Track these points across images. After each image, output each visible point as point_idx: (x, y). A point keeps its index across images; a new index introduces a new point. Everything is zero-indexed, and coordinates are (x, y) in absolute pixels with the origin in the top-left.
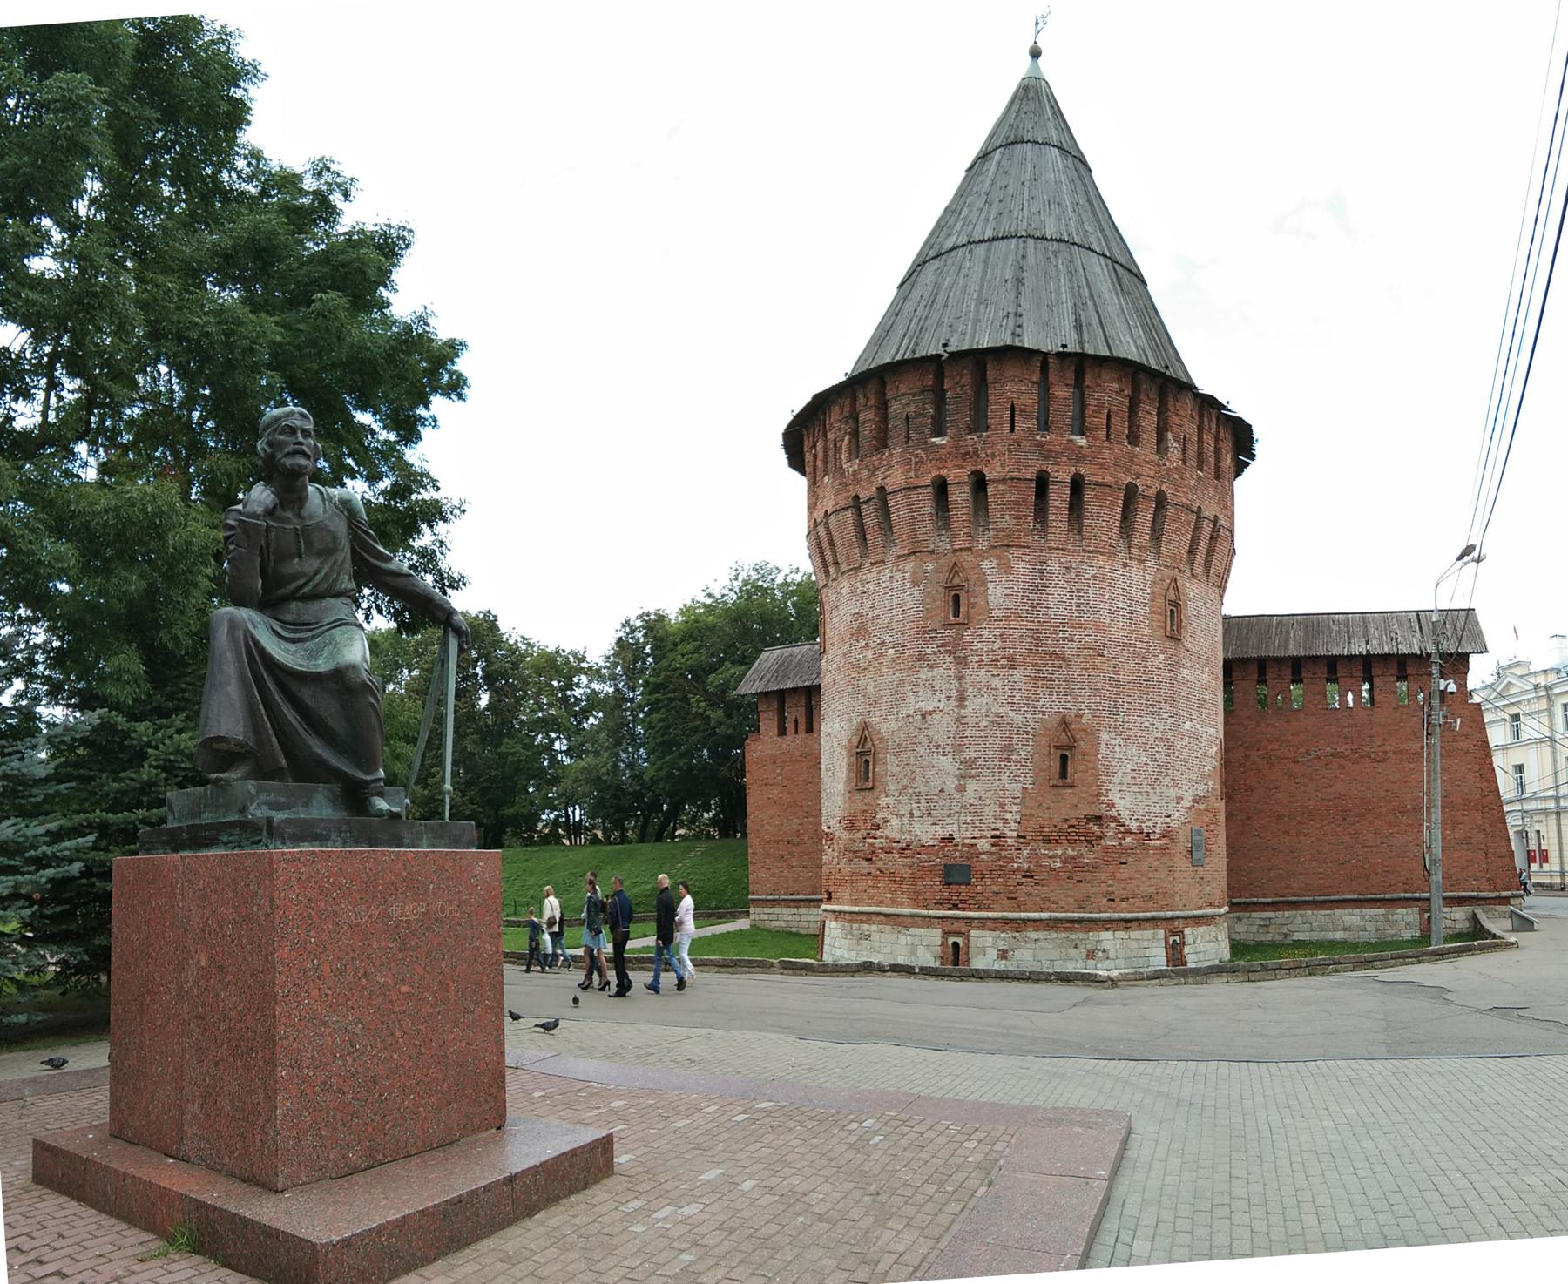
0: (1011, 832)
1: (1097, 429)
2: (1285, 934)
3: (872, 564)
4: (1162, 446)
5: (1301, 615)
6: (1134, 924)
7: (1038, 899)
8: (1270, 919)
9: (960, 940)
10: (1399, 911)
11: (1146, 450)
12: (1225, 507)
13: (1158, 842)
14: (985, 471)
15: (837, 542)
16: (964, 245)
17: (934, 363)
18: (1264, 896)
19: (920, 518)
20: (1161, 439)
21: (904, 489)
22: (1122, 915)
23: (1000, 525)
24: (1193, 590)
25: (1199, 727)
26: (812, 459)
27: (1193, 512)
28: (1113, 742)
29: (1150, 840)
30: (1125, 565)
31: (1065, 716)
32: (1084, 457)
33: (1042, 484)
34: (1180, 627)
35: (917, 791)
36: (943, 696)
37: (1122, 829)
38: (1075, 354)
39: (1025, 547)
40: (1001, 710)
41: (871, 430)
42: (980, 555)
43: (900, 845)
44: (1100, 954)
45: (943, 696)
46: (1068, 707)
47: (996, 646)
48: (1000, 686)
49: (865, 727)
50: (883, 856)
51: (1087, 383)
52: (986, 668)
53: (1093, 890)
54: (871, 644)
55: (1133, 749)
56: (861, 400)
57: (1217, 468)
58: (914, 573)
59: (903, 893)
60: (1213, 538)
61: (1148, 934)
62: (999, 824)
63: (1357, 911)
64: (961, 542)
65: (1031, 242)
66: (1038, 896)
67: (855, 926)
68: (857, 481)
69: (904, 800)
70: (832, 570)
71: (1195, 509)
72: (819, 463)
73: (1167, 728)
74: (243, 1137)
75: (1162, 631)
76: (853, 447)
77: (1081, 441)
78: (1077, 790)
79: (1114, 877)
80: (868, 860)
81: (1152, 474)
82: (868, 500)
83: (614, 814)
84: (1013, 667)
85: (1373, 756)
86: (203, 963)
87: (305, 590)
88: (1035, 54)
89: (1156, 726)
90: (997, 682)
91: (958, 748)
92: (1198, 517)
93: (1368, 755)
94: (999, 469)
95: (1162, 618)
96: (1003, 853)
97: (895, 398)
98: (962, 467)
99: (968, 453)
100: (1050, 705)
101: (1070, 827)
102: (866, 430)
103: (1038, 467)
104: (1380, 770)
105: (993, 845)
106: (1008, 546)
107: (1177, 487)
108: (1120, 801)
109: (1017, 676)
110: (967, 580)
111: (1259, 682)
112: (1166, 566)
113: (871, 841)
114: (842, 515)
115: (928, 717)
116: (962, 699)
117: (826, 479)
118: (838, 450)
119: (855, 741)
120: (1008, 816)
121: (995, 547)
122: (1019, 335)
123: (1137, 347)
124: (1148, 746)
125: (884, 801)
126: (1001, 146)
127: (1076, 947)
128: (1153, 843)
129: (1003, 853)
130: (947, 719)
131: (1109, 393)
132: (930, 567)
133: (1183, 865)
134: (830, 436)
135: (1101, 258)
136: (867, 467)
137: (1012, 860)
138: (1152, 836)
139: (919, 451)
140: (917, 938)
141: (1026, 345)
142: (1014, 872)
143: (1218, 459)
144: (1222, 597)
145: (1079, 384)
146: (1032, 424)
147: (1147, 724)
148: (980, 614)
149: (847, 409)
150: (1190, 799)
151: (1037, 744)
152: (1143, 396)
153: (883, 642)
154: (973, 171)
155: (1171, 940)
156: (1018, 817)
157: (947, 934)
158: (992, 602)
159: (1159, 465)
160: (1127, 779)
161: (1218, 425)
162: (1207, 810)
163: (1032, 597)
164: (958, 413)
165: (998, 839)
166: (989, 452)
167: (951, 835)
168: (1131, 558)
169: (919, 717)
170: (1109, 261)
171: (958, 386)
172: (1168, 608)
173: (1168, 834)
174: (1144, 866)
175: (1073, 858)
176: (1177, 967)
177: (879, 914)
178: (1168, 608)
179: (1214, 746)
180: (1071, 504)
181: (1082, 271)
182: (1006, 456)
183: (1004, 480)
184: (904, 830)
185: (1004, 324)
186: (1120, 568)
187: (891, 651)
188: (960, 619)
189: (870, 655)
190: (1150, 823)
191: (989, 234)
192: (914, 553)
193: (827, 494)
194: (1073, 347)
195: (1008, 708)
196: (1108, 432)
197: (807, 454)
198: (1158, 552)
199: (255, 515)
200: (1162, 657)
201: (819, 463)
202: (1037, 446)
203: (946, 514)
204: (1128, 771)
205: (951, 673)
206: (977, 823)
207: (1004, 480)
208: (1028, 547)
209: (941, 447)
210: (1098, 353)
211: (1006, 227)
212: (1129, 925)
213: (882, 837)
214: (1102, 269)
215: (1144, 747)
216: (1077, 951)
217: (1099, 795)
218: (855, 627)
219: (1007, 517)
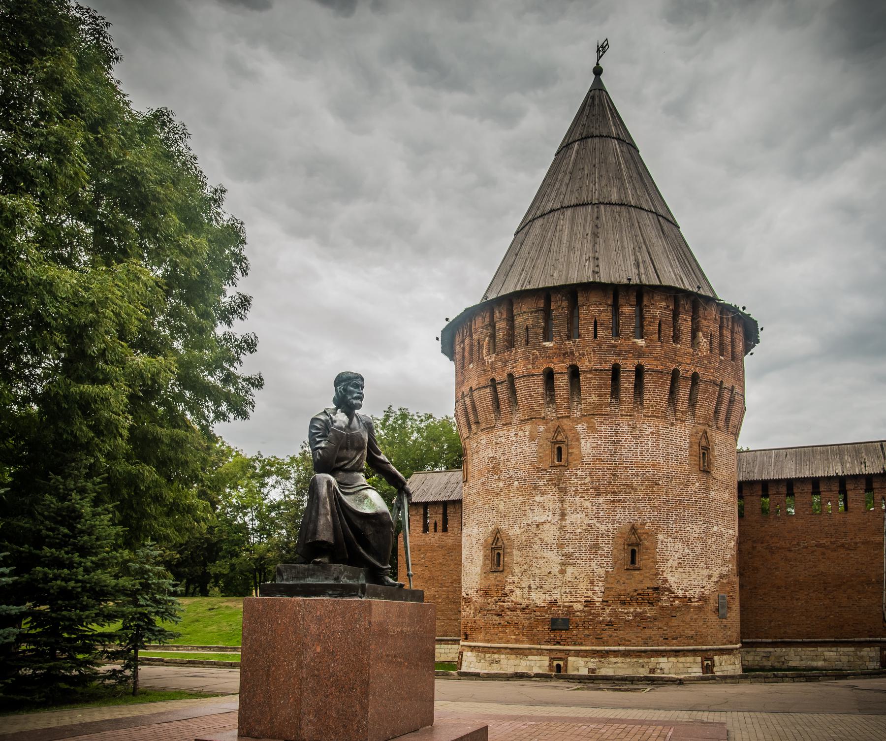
0: (598, 598)
1: (652, 334)
3: (504, 425)
4: (695, 342)
5: (792, 448)
6: (681, 653)
7: (616, 639)
9: (561, 663)
10: (865, 649)
11: (684, 347)
12: (739, 380)
13: (697, 604)
14: (579, 364)
16: (558, 209)
17: (546, 294)
18: (767, 638)
20: (694, 336)
21: (525, 376)
22: (673, 648)
23: (588, 401)
24: (718, 438)
25: (722, 529)
26: (461, 351)
27: (717, 385)
30: (672, 424)
31: (633, 525)
32: (644, 353)
33: (616, 371)
34: (710, 463)
37: (673, 595)
38: (637, 285)
39: (605, 415)
40: (591, 522)
41: (504, 335)
42: (575, 421)
43: (522, 606)
44: (659, 671)
46: (636, 518)
47: (587, 481)
48: (590, 507)
49: (497, 532)
50: (509, 613)
51: (644, 303)
53: (654, 633)
54: (502, 478)
55: (679, 545)
57: (733, 352)
58: (531, 432)
60: (731, 402)
61: (690, 659)
62: (590, 594)
63: (834, 649)
64: (562, 412)
65: (602, 207)
66: (616, 636)
67: (487, 655)
68: (493, 369)
69: (525, 578)
70: (473, 427)
71: (718, 383)
72: (466, 354)
75: (697, 467)
76: (491, 346)
77: (641, 342)
78: (642, 572)
79: (667, 625)
80: (499, 615)
81: (689, 362)
82: (502, 382)
84: (599, 494)
85: (847, 546)
86: (318, 650)
89: (695, 530)
90: (587, 504)
91: (560, 546)
92: (721, 388)
93: (843, 546)
94: (587, 364)
95: (697, 459)
96: (593, 611)
97: (519, 314)
98: (563, 362)
99: (567, 353)
100: (624, 518)
101: (638, 594)
102: (500, 335)
103: (613, 362)
104: (852, 555)
105: (585, 606)
106: (593, 415)
107: (706, 369)
109: (601, 500)
110: (566, 437)
111: (762, 496)
112: (699, 424)
113: (501, 604)
114: (482, 392)
115: (541, 527)
116: (563, 515)
117: (471, 366)
118: (480, 347)
119: (490, 540)
120: (596, 588)
121: (585, 415)
122: (597, 273)
123: (675, 275)
125: (510, 579)
126: (578, 140)
127: (643, 667)
128: (693, 604)
129: (593, 611)
130: (554, 527)
131: (658, 309)
132: (542, 428)
133: (713, 618)
134: (475, 337)
135: (650, 214)
136: (501, 360)
137: (599, 615)
139: (535, 351)
141: (603, 281)
142: (600, 622)
143: (733, 347)
144: (736, 440)
147: (688, 529)
149: (487, 320)
150: (717, 576)
151: (615, 543)
152: (681, 309)
153: (511, 477)
154: (560, 156)
155: (706, 663)
156: (603, 589)
157: (552, 660)
158: (584, 452)
159: (693, 355)
160: (675, 564)
162: (728, 583)
163: (611, 448)
164: (559, 325)
165: (589, 603)
168: (676, 420)
169: (535, 526)
170: (655, 216)
171: (559, 307)
172: (702, 451)
173: (703, 599)
174: (688, 619)
175: (640, 613)
176: (709, 675)
177: (506, 648)
178: (702, 451)
180: (635, 385)
181: (637, 224)
183: (590, 371)
185: (587, 264)
187: (516, 483)
188: (562, 463)
189: (501, 484)
190: (691, 592)
191: (573, 202)
192: (531, 419)
194: (635, 281)
195: (595, 521)
196: (659, 335)
197: (458, 347)
198: (694, 415)
199: (341, 428)
200: (697, 484)
201: (466, 354)
203: (552, 393)
204: (676, 558)
205: (556, 498)
206: (573, 593)
207: (590, 371)
208: (607, 415)
209: (550, 348)
210: (651, 283)
211: (584, 197)
212: (678, 654)
213: (509, 602)
214: (650, 221)
215: (687, 543)
216: (644, 669)
217: (657, 574)
218: (491, 466)
219: (593, 396)
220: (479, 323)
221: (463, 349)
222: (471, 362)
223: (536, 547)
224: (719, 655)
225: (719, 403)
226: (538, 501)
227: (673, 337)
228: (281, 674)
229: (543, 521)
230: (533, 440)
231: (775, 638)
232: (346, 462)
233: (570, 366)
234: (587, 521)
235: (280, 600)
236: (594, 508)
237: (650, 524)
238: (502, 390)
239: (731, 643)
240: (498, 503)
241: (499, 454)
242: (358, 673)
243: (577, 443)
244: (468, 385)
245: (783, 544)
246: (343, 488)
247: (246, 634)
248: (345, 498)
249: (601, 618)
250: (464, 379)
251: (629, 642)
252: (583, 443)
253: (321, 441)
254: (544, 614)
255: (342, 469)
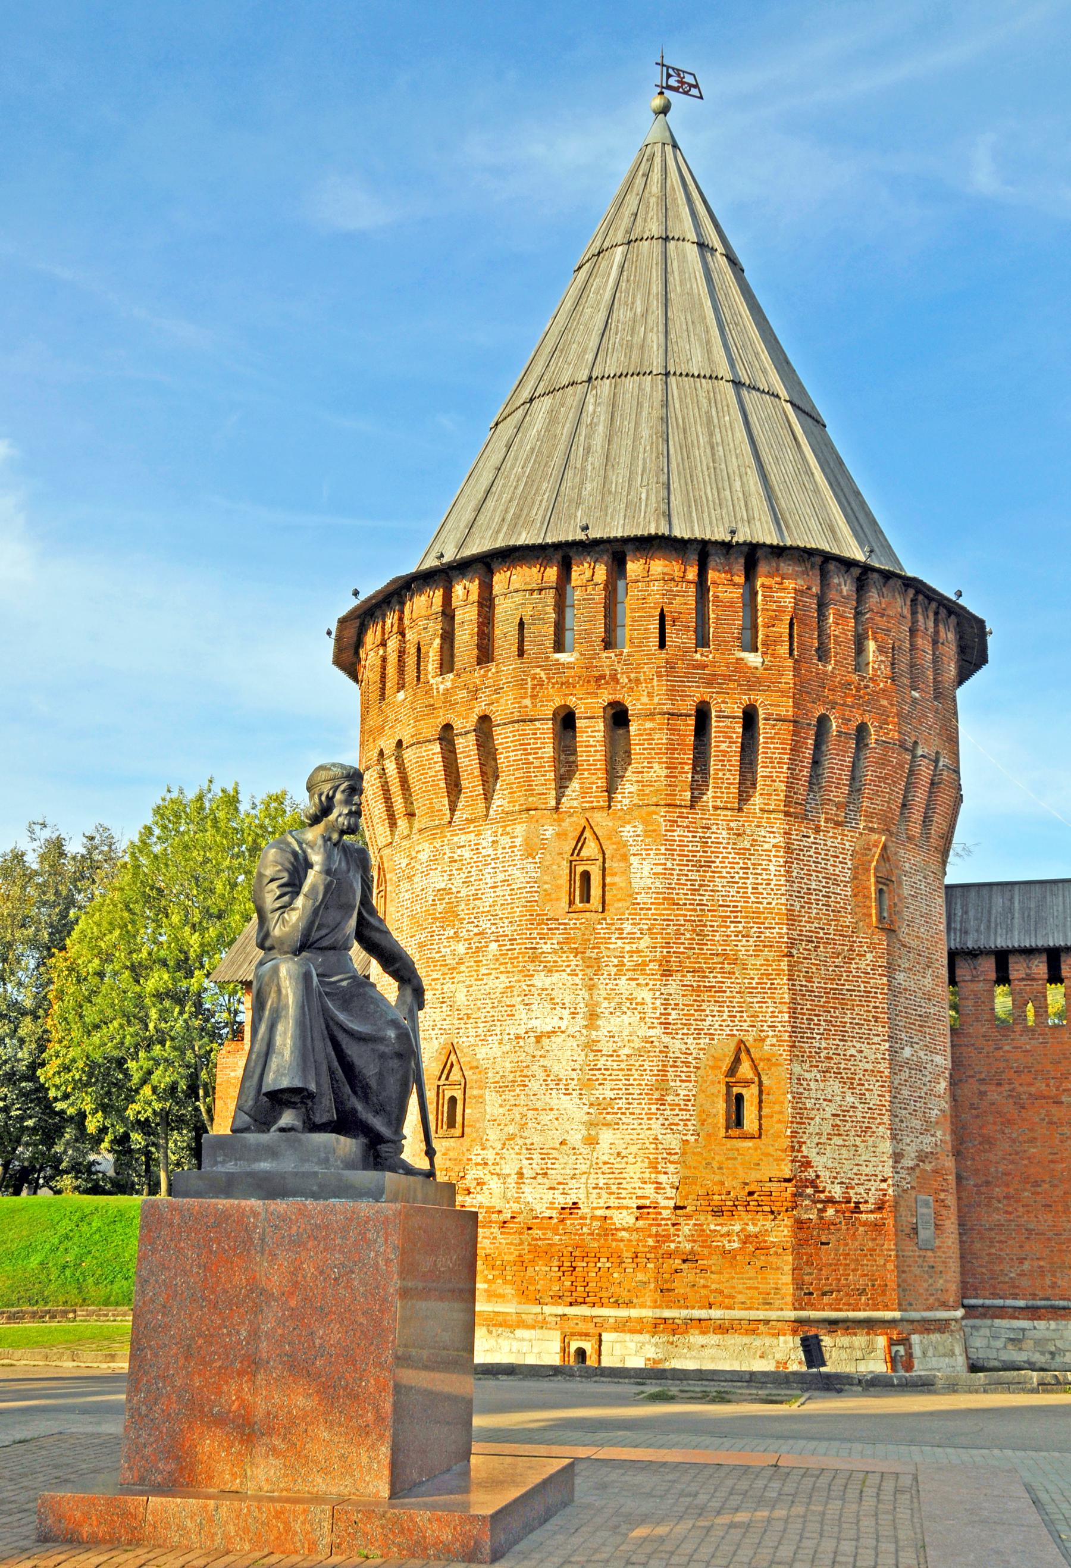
2: (1052, 1354)
8: (1023, 1330)
13: (872, 1217)
15: (415, 786)
18: (1015, 1296)
19: (537, 763)
21: (518, 721)
24: (910, 859)
25: (921, 1054)
27: (907, 750)
28: (808, 1076)
29: (861, 1213)
33: (702, 716)
34: (896, 912)
35: (528, 1141)
36: (567, 1011)
40: (652, 1032)
43: (502, 1217)
45: (567, 1011)
48: (648, 1000)
52: (629, 974)
54: (464, 934)
56: (458, 590)
59: (505, 1282)
61: (860, 1340)
66: (705, 1287)
70: (402, 823)
71: (909, 745)
73: (879, 1056)
77: (753, 659)
83: (250, 1551)
84: (667, 973)
91: (587, 1084)
94: (645, 699)
99: (603, 677)
108: (818, 1158)
109: (673, 986)
115: (545, 1041)
116: (593, 1016)
117: (401, 695)
120: (663, 1178)
124: (856, 1082)
125: (477, 1154)
128: (864, 1216)
137: (667, 1238)
138: (862, 1207)
139: (538, 670)
140: (526, 1343)
142: (670, 1255)
143: (937, 671)
146: (689, 639)
147: (853, 1051)
148: (619, 900)
150: (913, 1155)
156: (675, 1180)
160: (827, 1128)
161: (936, 625)
162: (935, 1171)
163: (693, 876)
166: (633, 676)
167: (574, 1203)
169: (533, 1040)
179: (941, 1080)
182: (655, 683)
184: (509, 1195)
186: (810, 833)
187: (494, 946)
189: (461, 948)
190: (861, 1190)
193: (401, 717)
200: (869, 956)
202: (696, 667)
203: (572, 758)
204: (828, 1116)
205: (577, 980)
206: (614, 1188)
209: (570, 666)
215: (850, 1083)
218: (440, 908)
219: (656, 766)
221: (384, 659)
222: (401, 687)
223: (534, 1085)
224: (921, 1333)
225: (909, 787)
226: (539, 985)
227: (818, 650)
228: (215, 1353)
229: (549, 1029)
230: (530, 855)
231: (1034, 1296)
233: (611, 704)
234: (643, 1031)
236: (658, 1002)
237: (774, 1040)
238: (466, 746)
239: (944, 1305)
240: (453, 987)
241: (458, 881)
243: (622, 864)
244: (392, 736)
245: (1043, 1087)
247: (144, 1273)
249: (673, 1246)
250: (385, 721)
251: (726, 1300)
252: (635, 865)
254: (549, 1235)
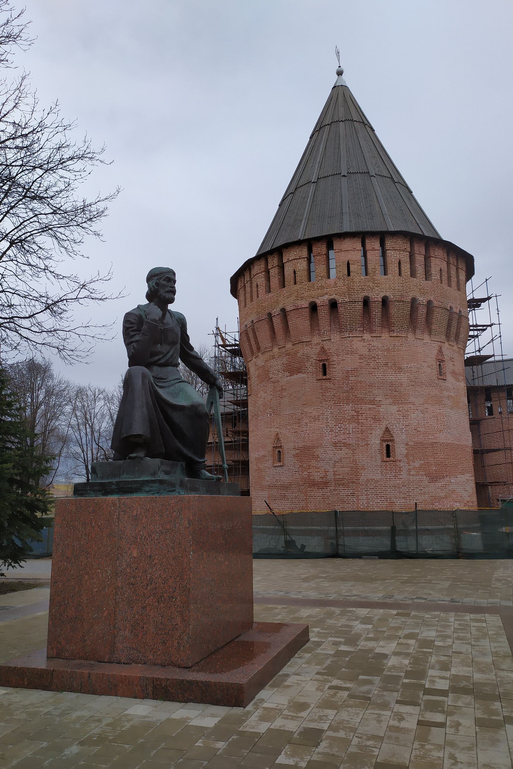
74: (164, 643)
86: (135, 554)
87: (162, 361)
88: (340, 73)
145: (382, 244)
199: (155, 320)
220: (258, 268)
228: (94, 583)
232: (161, 356)
235: (94, 500)
238: (277, 322)
242: (178, 579)
246: (158, 382)
248: (161, 391)
253: (135, 335)
255: (155, 363)
